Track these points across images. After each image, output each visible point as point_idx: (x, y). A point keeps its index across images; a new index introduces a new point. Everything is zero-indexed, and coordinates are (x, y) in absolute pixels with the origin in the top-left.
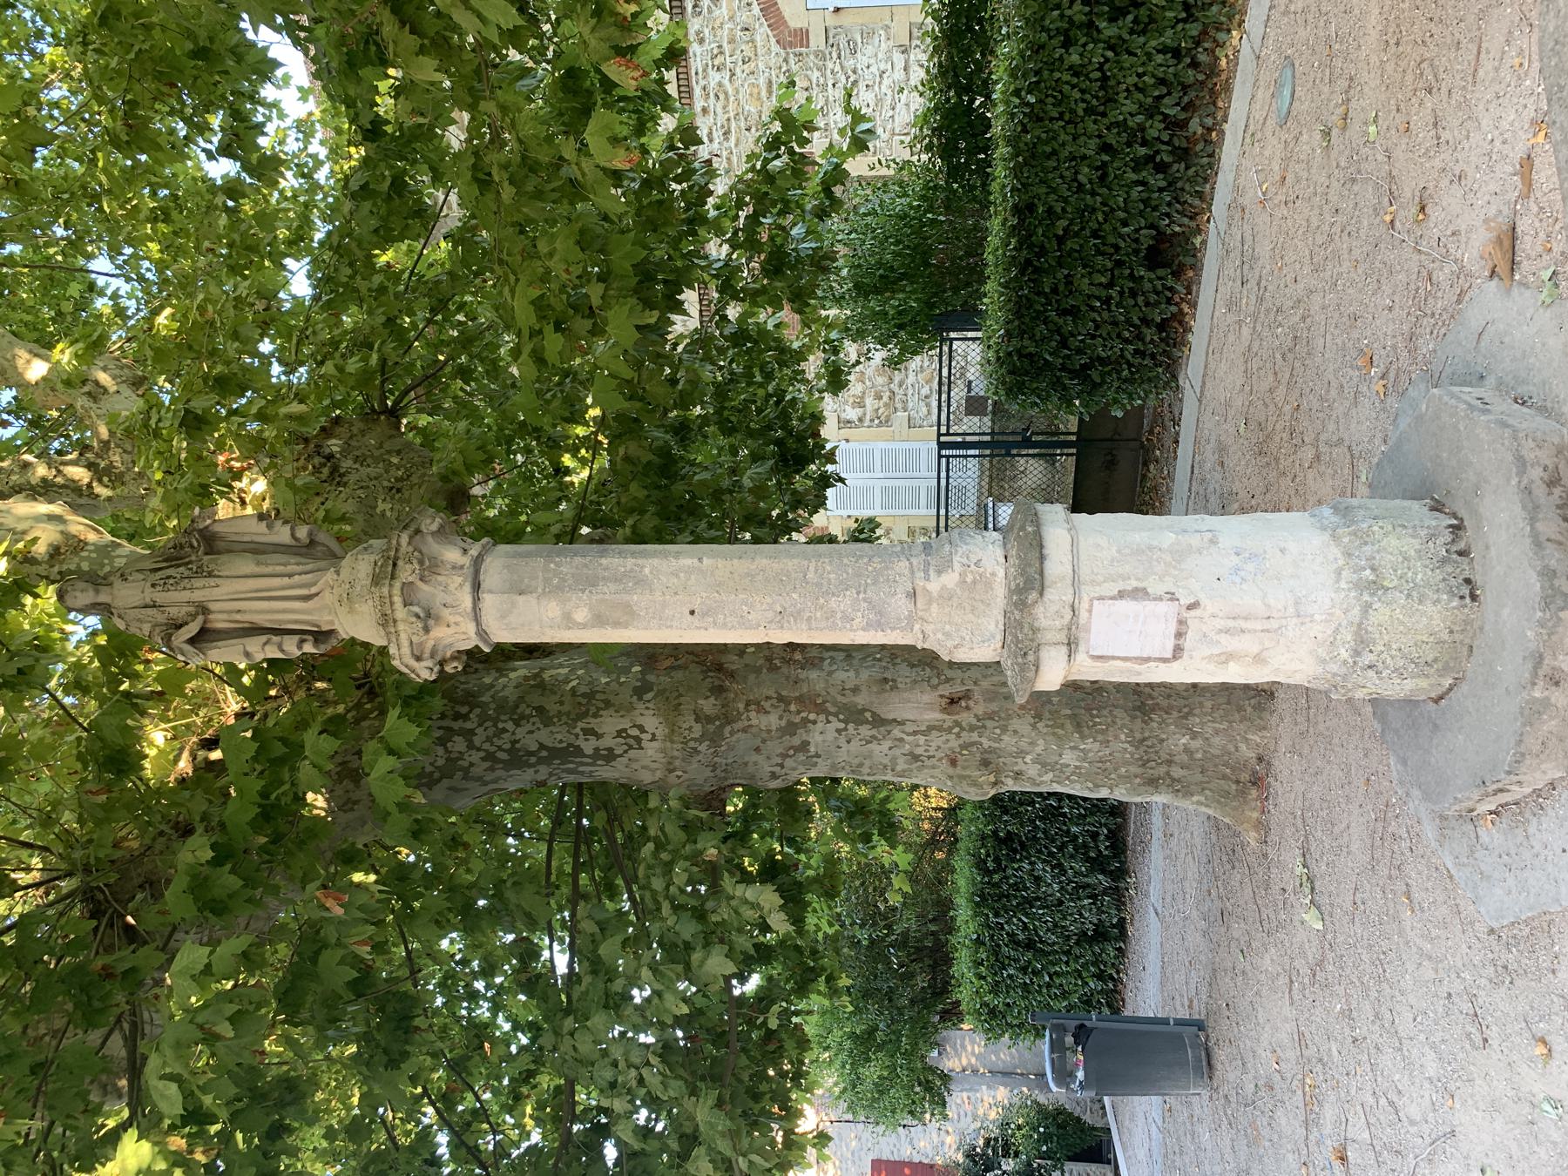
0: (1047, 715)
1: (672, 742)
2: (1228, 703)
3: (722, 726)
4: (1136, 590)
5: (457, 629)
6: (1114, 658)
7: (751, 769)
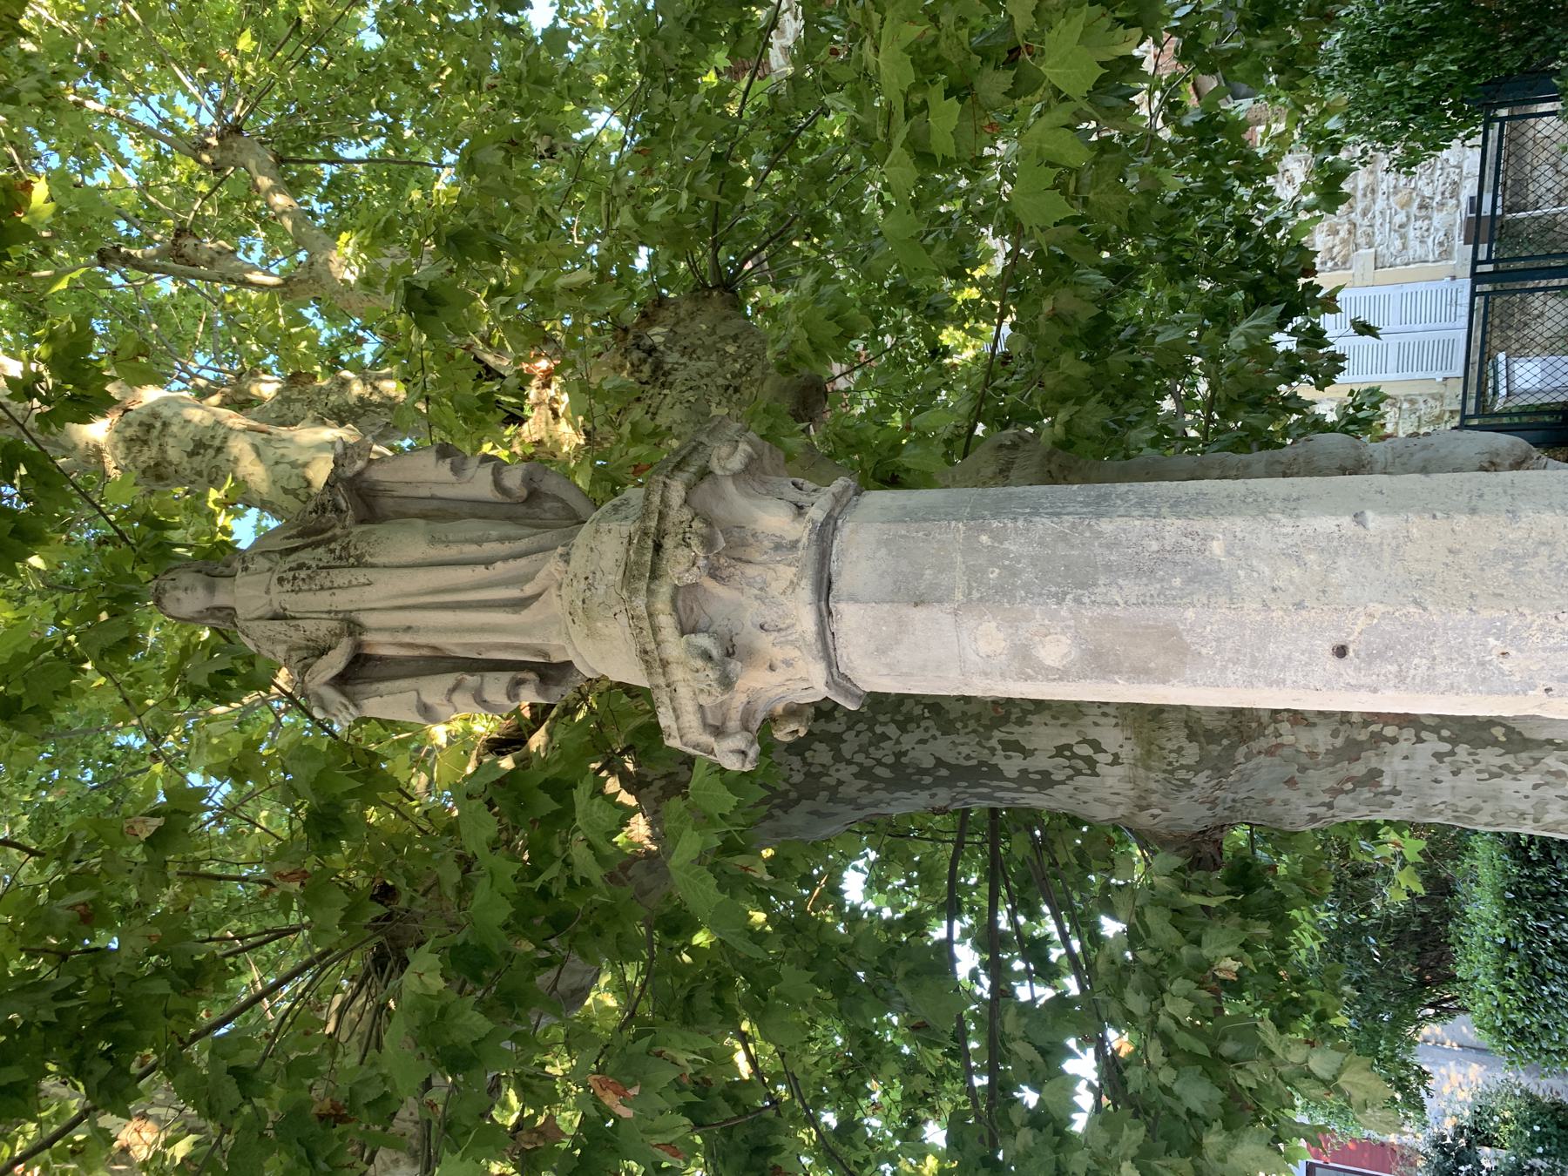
1: (1148, 768)
3: (1233, 747)
5: (790, 673)
7: (1276, 809)
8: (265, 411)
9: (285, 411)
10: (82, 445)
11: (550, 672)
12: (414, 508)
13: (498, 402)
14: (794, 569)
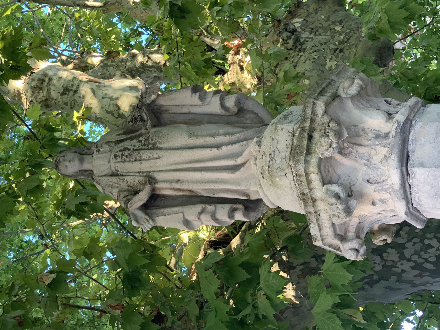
5: (384, 207)
8: (95, 72)
9: (105, 71)
10: (12, 91)
11: (251, 205)
12: (180, 118)
13: (213, 63)
14: (387, 149)
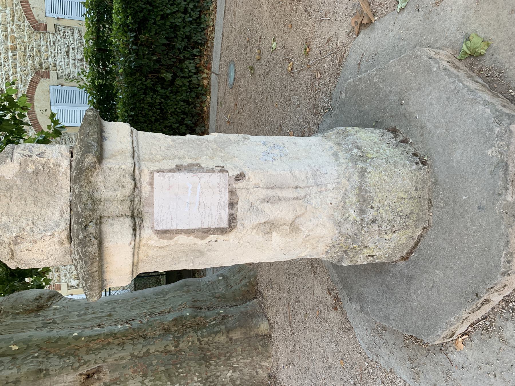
0: (150, 373)
2: (249, 346)
4: (191, 165)
6: (178, 232)
